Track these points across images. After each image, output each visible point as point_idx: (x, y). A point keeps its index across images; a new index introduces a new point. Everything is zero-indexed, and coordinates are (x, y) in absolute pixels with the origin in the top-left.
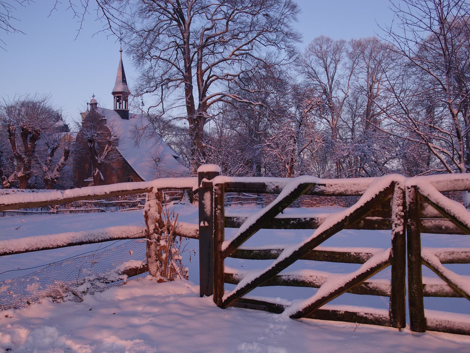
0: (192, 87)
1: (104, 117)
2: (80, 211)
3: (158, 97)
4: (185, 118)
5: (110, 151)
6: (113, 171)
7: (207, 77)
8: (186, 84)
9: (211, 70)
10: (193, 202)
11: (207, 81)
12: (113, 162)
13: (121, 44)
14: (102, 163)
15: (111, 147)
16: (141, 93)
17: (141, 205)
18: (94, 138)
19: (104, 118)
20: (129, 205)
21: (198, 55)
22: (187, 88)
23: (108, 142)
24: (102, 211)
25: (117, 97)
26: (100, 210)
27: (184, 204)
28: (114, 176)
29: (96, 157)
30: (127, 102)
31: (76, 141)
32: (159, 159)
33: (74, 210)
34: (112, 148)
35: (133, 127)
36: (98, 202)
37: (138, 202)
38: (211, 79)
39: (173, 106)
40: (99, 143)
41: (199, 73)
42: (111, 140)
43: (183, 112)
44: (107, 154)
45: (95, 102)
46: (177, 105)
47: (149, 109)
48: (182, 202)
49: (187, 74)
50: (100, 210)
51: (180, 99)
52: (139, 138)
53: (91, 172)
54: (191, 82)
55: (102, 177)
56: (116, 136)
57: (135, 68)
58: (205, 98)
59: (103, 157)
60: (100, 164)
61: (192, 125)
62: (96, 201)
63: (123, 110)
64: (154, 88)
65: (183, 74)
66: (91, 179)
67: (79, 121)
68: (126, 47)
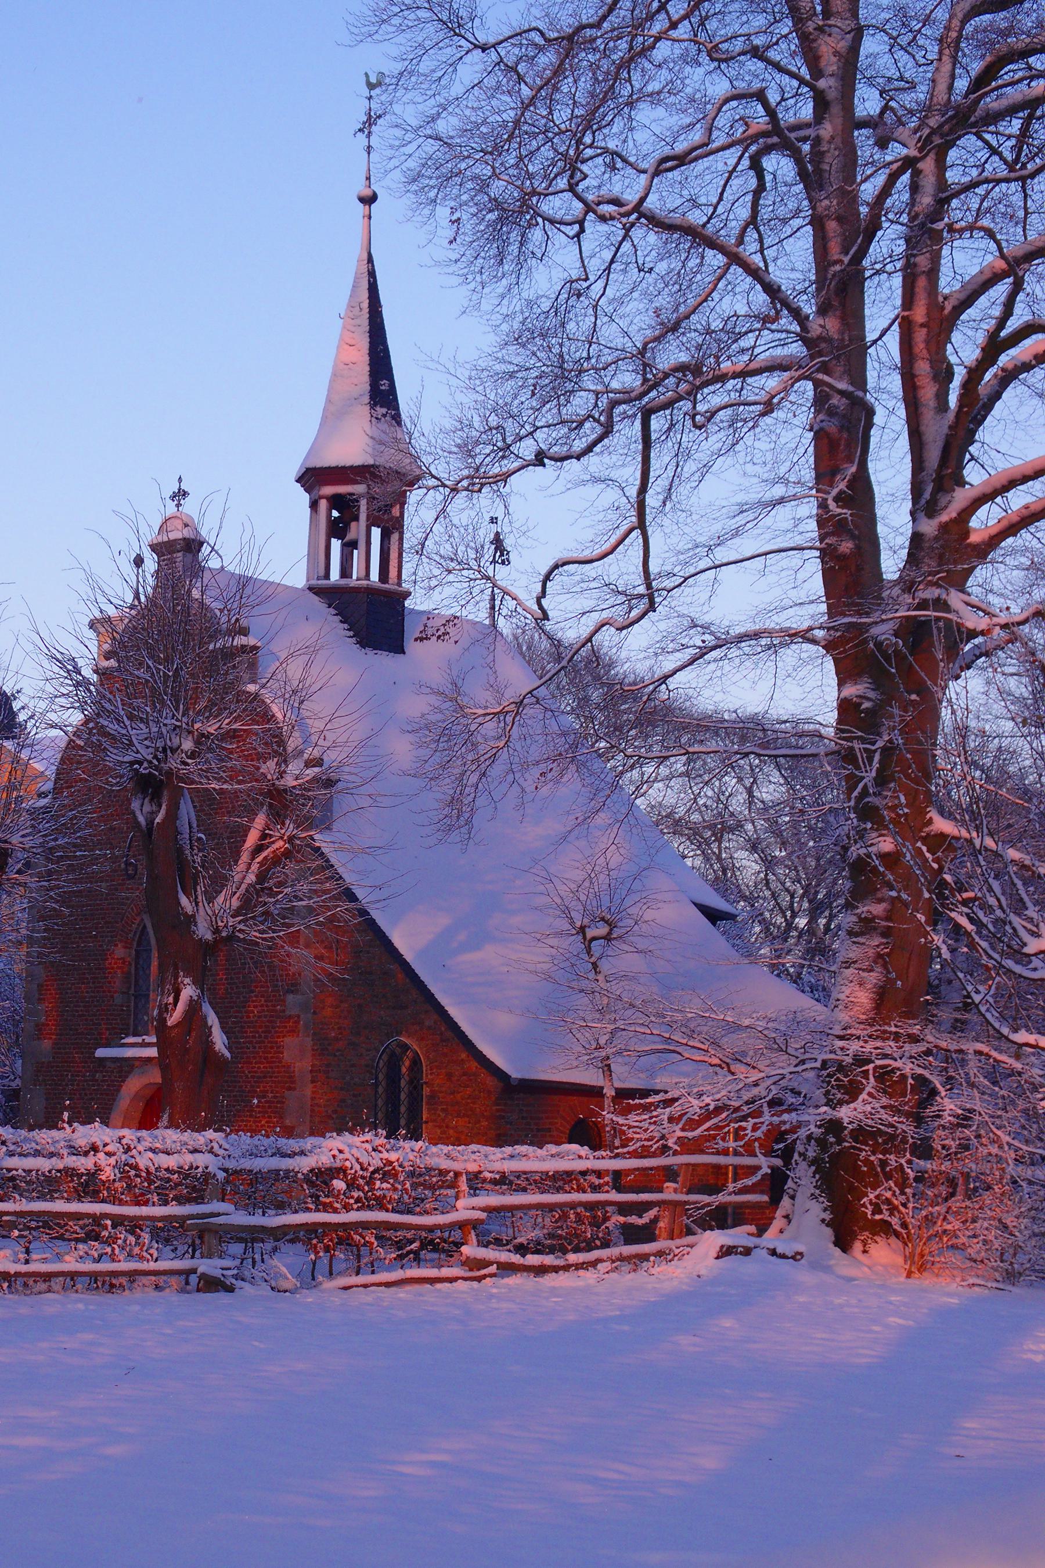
0: (871, 412)
1: (244, 632)
2: (57, 1283)
3: (612, 495)
4: (805, 636)
5: (276, 860)
6: (290, 998)
7: (981, 338)
8: (820, 401)
9: (1018, 287)
10: (858, 1246)
11: (975, 373)
12: (294, 939)
13: (369, 149)
14: (223, 942)
15: (290, 829)
16: (496, 470)
17: (483, 1253)
18: (173, 763)
19: (240, 641)
20: (399, 1245)
21: (914, 188)
22: (832, 426)
23: (270, 794)
24: (211, 1284)
25: (336, 501)
26: (193, 1279)
27: (797, 1256)
28: (293, 1032)
29: (184, 900)
30: (395, 537)
31: (57, 791)
32: (611, 925)
33: (13, 1268)
34: (291, 839)
35: (434, 700)
36: (182, 1219)
37: (462, 1225)
38: (1004, 359)
39: (721, 555)
40: (205, 801)
41: (919, 314)
42: (289, 781)
43: (793, 594)
44: (261, 877)
45: (187, 533)
46: (746, 545)
47: (547, 578)
48: (770, 1238)
49: (832, 325)
50: (193, 1279)
51: (781, 501)
52: (474, 778)
53: (141, 997)
54: (859, 380)
55: (219, 1040)
56: (318, 762)
57: (464, 291)
58: (960, 498)
59: (227, 901)
60: (209, 949)
61: (851, 691)
62: (174, 1209)
63: (370, 591)
64: (591, 430)
65: (804, 328)
66: (144, 1045)
67: (74, 648)
68: (409, 149)
